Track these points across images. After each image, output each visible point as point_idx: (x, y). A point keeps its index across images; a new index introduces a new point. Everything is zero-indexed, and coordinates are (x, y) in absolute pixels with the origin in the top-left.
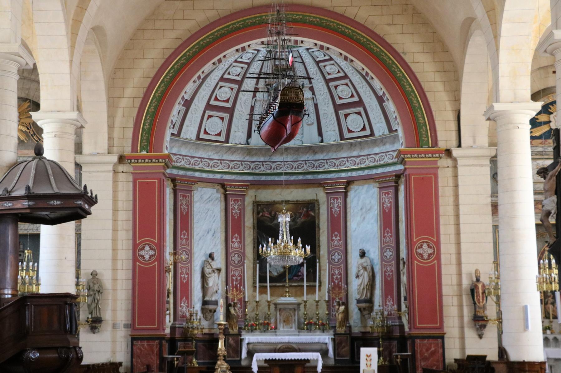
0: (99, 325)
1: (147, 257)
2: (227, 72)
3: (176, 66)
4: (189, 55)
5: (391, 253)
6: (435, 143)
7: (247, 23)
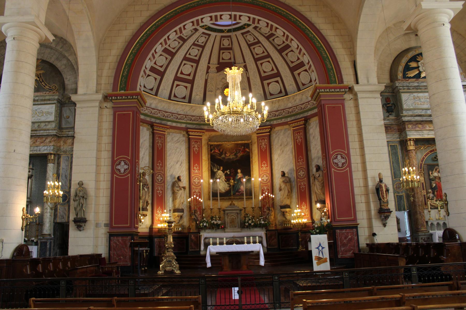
0: (83, 224)
1: (122, 171)
3: (148, 32)
4: (158, 25)
5: (303, 173)
6: (341, 81)
7: (200, 3)
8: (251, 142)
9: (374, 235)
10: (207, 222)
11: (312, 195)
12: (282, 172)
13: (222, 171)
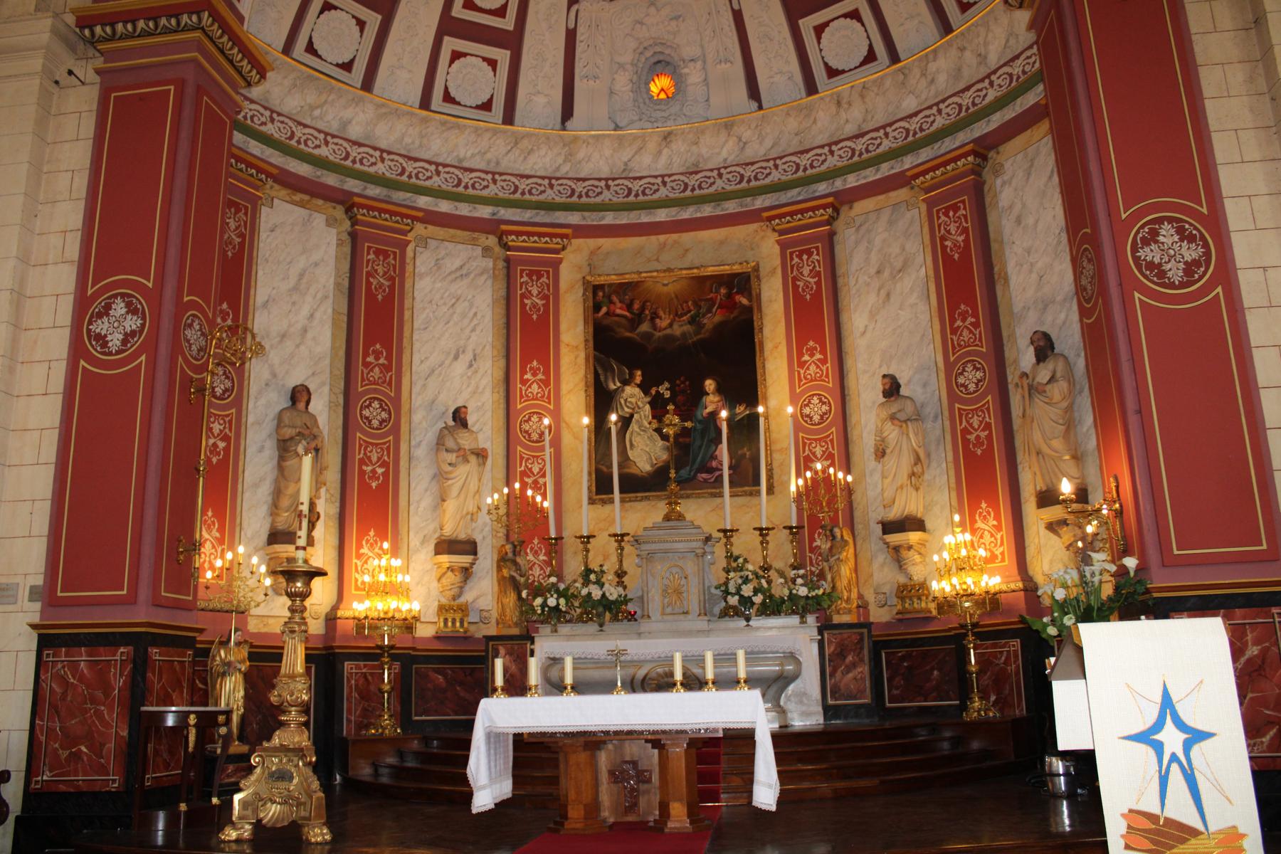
1: (115, 340)
5: (979, 375)
10: (561, 594)
11: (1020, 468)
12: (884, 376)
13: (639, 386)
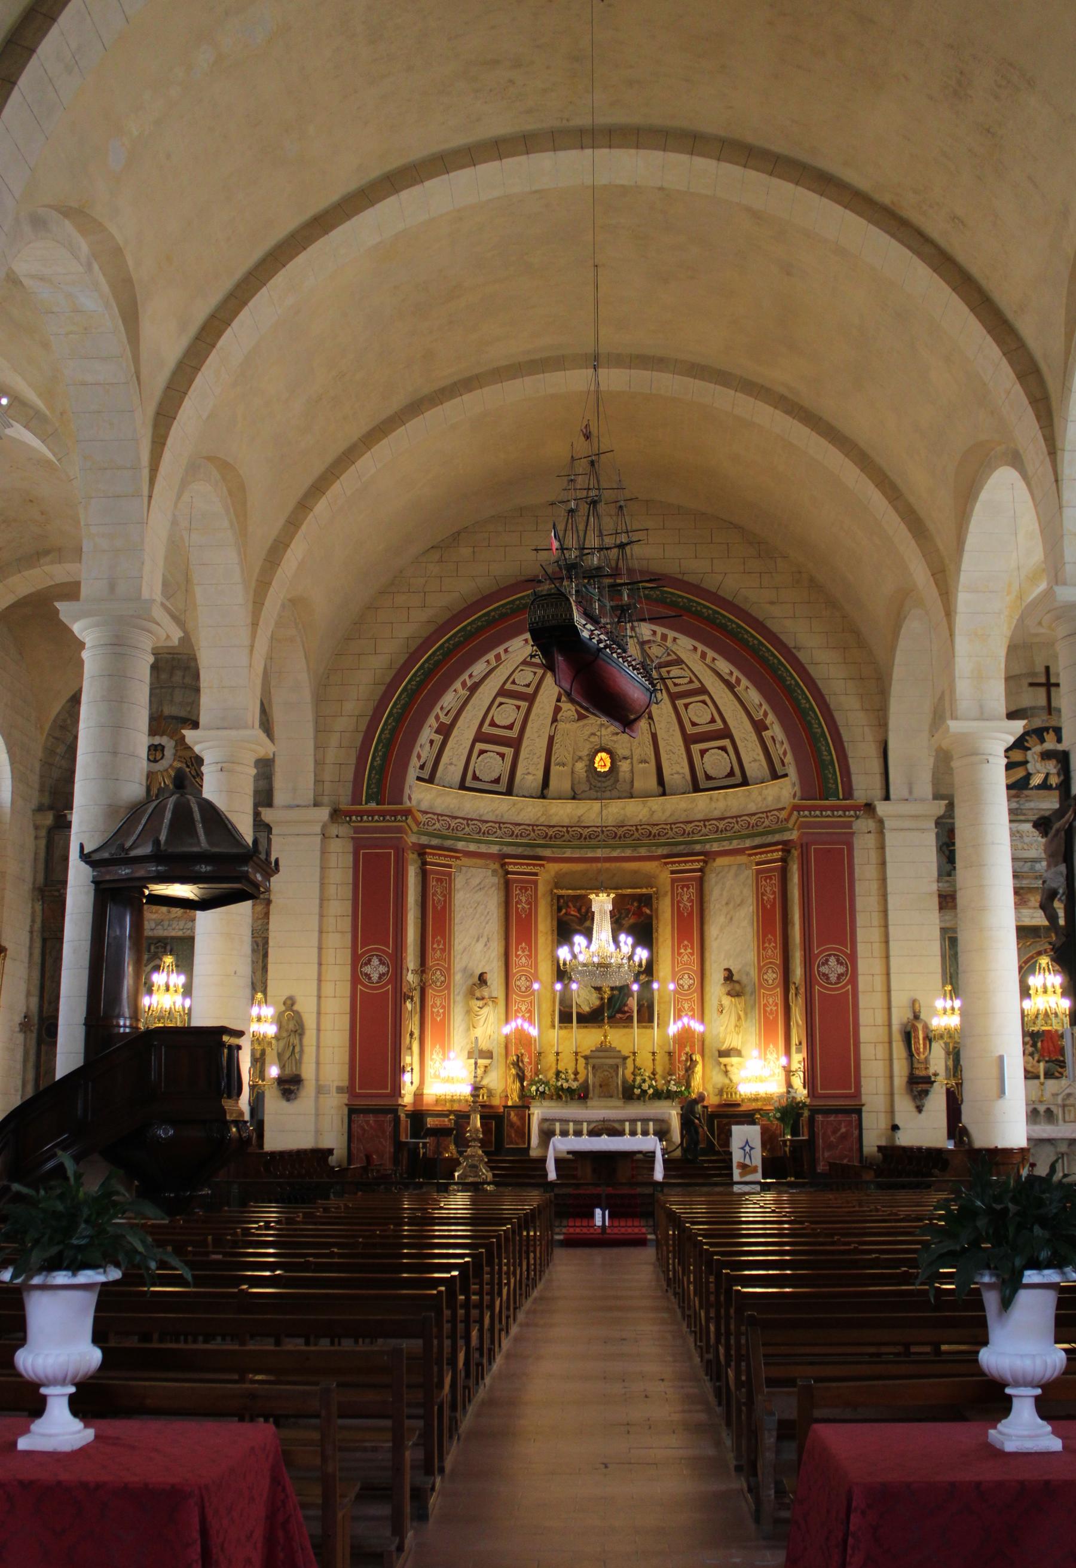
1: (375, 977)
2: (511, 680)
6: (849, 794)
8: (656, 893)
9: (895, 1128)
12: (725, 970)
